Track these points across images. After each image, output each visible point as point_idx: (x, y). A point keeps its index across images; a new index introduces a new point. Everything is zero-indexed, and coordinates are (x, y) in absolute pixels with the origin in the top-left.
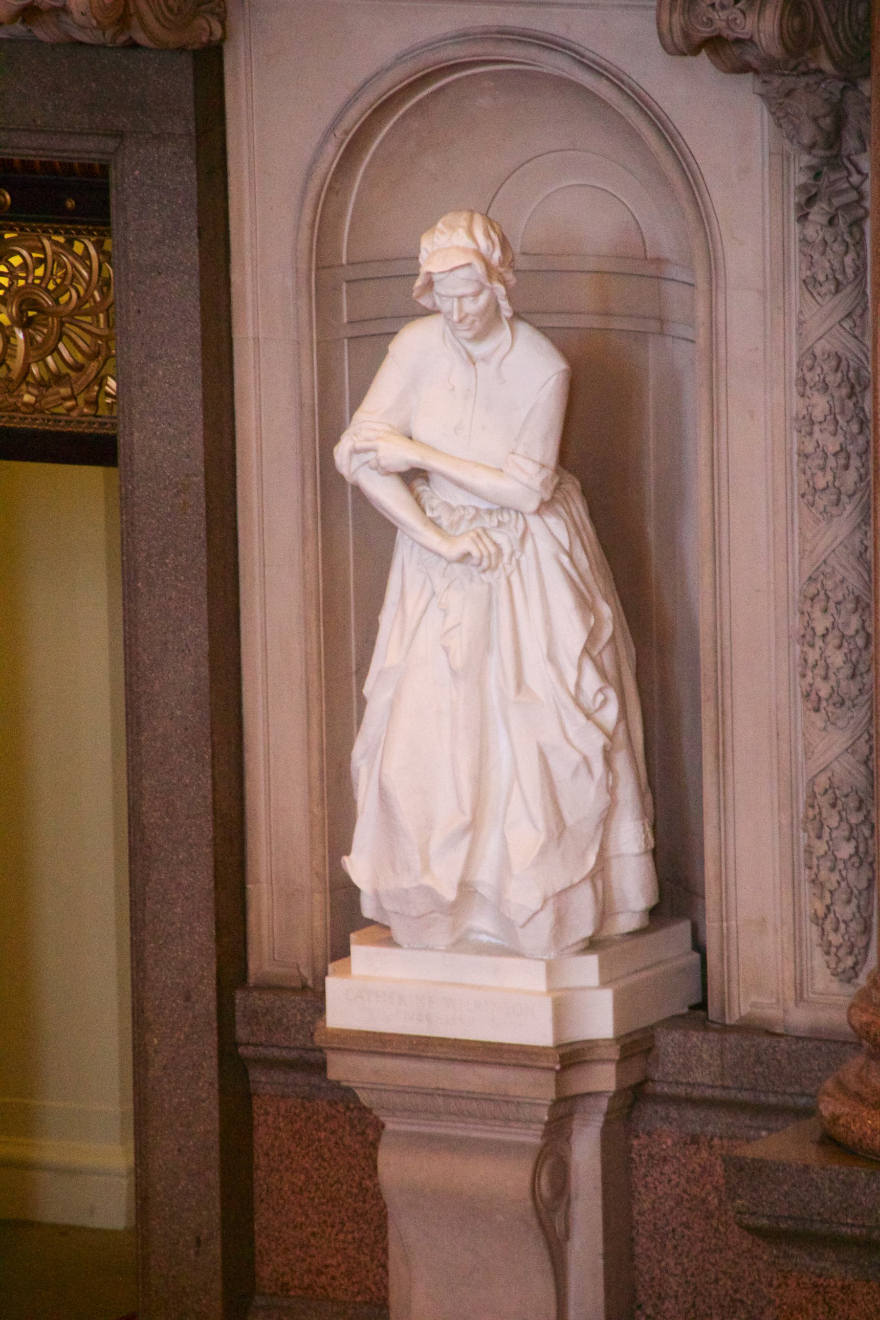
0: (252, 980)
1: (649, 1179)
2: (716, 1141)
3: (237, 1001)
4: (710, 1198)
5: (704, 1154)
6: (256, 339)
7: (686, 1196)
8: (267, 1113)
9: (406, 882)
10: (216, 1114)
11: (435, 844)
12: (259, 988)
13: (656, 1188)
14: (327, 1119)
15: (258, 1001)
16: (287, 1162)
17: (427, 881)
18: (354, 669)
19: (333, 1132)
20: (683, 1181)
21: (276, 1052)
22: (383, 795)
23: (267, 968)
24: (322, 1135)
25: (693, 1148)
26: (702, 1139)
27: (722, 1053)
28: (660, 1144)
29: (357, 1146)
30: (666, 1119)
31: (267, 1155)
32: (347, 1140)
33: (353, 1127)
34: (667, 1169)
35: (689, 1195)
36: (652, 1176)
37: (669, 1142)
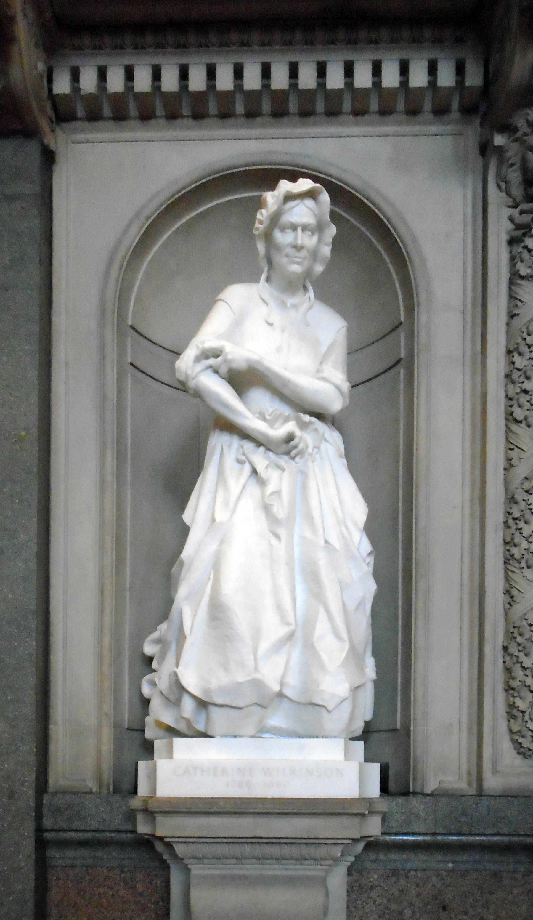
0: (51, 790)
1: (359, 902)
2: (412, 873)
3: (45, 802)
4: (405, 911)
5: (402, 882)
6: (67, 364)
7: (386, 911)
8: (58, 879)
9: (241, 677)
10: (32, 876)
11: (264, 646)
12: (55, 793)
13: (363, 908)
14: (106, 879)
15: (58, 801)
16: (73, 910)
17: (258, 676)
18: (128, 586)
19: (110, 888)
20: (385, 901)
21: (73, 834)
22: (218, 613)
23: (61, 782)
24: (101, 890)
25: (394, 879)
26: (402, 872)
27: (435, 811)
28: (368, 878)
29: (129, 896)
30: (375, 861)
31: (57, 906)
32: (122, 892)
33: (126, 883)
34: (373, 894)
35: (389, 910)
36: (361, 900)
37: (376, 877)
